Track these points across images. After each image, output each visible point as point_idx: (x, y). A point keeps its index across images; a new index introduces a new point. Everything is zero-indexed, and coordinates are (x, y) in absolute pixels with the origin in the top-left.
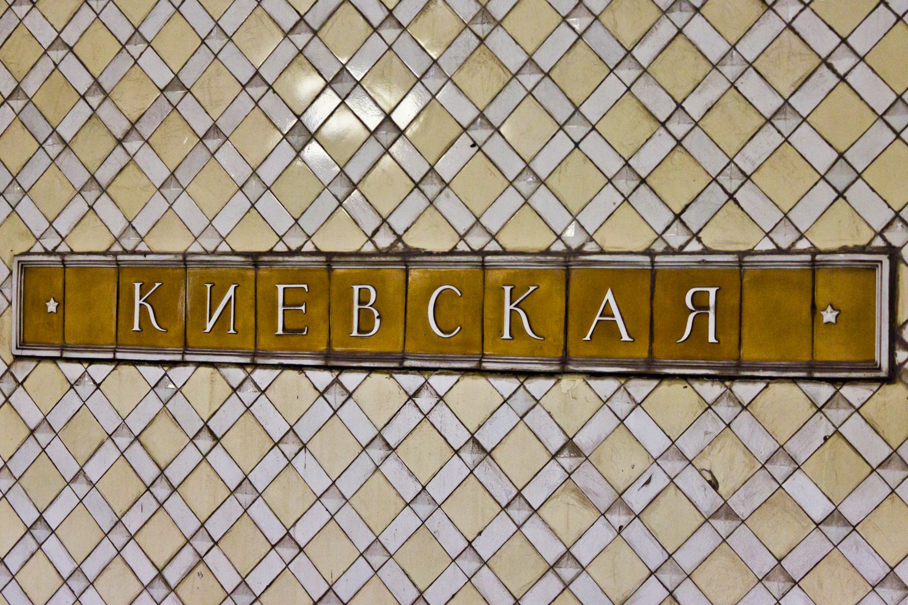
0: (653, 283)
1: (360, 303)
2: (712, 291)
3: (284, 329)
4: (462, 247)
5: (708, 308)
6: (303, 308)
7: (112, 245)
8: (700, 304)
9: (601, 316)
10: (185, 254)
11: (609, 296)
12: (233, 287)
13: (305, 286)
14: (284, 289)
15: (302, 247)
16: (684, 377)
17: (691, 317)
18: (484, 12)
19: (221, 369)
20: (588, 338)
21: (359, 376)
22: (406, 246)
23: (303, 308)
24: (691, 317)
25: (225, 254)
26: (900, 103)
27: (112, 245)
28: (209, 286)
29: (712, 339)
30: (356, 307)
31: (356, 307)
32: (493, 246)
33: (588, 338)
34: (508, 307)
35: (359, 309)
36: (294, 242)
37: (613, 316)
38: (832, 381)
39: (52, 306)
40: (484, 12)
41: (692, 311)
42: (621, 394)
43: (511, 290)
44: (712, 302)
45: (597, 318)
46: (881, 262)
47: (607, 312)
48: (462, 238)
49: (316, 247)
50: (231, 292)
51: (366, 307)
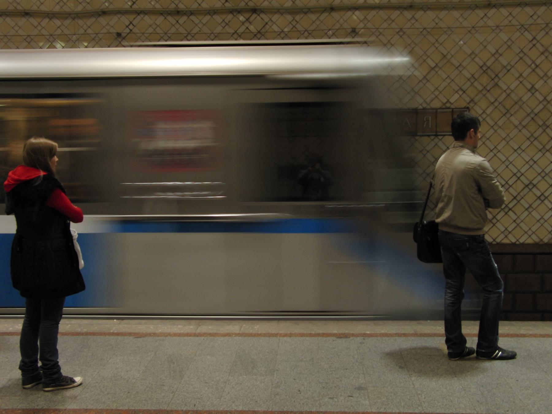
2: (430, 117)
29: (430, 127)
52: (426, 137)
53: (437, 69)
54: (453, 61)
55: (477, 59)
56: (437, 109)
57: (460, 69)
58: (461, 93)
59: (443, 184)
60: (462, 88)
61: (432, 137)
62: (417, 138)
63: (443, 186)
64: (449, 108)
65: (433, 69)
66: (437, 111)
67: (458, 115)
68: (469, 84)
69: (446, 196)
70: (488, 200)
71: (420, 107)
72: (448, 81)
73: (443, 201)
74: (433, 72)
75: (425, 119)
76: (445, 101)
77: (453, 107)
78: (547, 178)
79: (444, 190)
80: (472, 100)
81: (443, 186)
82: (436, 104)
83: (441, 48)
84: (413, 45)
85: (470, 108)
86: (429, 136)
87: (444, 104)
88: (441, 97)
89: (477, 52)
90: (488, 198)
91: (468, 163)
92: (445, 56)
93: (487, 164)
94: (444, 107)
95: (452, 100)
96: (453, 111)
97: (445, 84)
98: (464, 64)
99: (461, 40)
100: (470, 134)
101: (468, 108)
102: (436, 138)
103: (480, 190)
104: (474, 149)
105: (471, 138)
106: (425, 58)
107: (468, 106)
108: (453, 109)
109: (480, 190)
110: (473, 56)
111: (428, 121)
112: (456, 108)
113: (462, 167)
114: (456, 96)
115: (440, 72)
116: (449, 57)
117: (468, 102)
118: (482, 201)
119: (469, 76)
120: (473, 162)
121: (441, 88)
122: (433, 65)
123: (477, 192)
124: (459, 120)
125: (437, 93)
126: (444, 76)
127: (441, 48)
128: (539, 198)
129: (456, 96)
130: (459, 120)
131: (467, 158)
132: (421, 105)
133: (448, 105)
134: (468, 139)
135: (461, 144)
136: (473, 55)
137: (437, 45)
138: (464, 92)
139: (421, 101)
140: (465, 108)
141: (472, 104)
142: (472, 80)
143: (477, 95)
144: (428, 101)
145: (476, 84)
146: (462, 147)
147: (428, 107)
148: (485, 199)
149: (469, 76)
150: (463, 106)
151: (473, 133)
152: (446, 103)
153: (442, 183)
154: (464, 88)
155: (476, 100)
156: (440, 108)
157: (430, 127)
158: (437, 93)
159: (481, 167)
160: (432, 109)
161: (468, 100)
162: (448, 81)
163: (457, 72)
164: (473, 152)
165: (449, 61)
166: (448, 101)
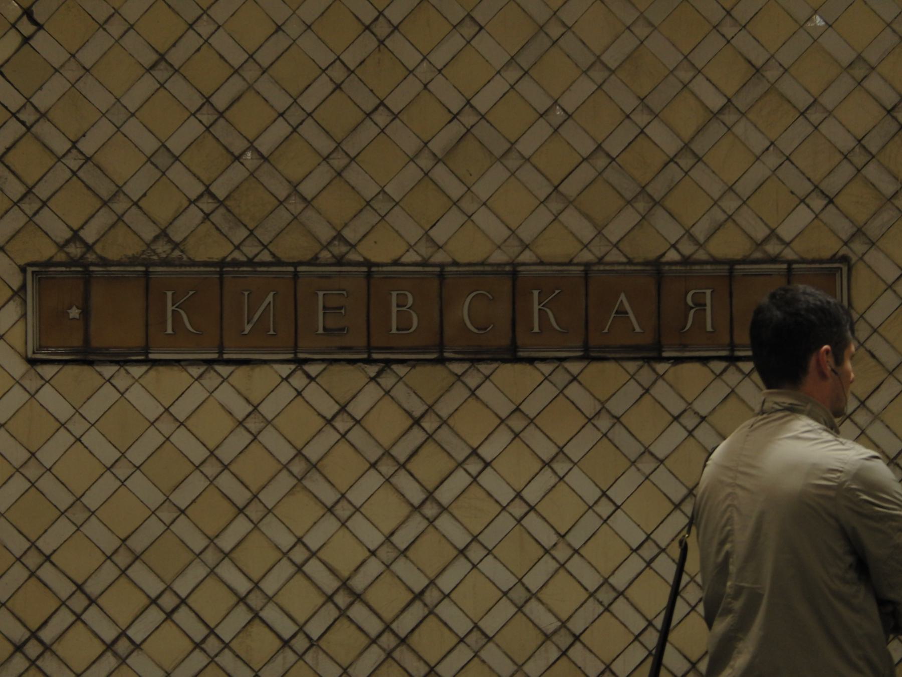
0: (584, 285)
1: (398, 306)
2: (708, 292)
3: (325, 329)
4: (237, 255)
5: (705, 305)
6: (343, 311)
10: (514, 264)
11: (623, 297)
12: (272, 294)
15: (663, 255)
16: (178, 362)
18: (28, 13)
19: (127, 368)
28: (246, 293)
29: (709, 328)
30: (394, 309)
31: (394, 309)
32: (266, 257)
33: (606, 331)
34: (170, 308)
36: (250, 250)
40: (28, 13)
41: (692, 308)
42: (299, 373)
43: (173, 294)
44: (708, 302)
45: (613, 315)
46: (841, 269)
48: (237, 248)
49: (537, 256)
50: (270, 298)
51: (404, 309)
52: (696, 367)
53: (729, 118)
54: (788, 87)
55: (874, 84)
56: (732, 263)
57: (815, 116)
58: (818, 203)
59: (727, 547)
60: (823, 186)
61: (718, 366)
62: (661, 367)
63: (728, 555)
64: (774, 260)
65: (715, 115)
66: (731, 271)
67: (773, 296)
68: (847, 170)
69: (738, 592)
70: (892, 603)
71: (673, 256)
72: (772, 160)
73: (728, 611)
74: (716, 130)
75: (690, 302)
76: (760, 233)
77: (789, 254)
78: (18, 633)
79: (733, 569)
80: (859, 232)
81: (728, 555)
82: (729, 246)
83: (743, 41)
84: (641, 30)
85: (854, 259)
86: (704, 360)
87: (759, 245)
88: (746, 219)
89: (872, 57)
90: (892, 596)
91: (815, 469)
92: (758, 71)
93: (882, 471)
94: (758, 255)
95: (787, 231)
96: (789, 270)
97: (760, 172)
98: (828, 100)
99: (816, 12)
100: (818, 361)
101: (845, 259)
102: (732, 369)
103: (862, 567)
104: (833, 418)
105: (823, 376)
106: (685, 75)
107: (845, 251)
108: (790, 263)
109: (862, 567)
110: (859, 72)
111: (701, 305)
112: (803, 261)
113: (794, 483)
114: (803, 216)
115: (739, 129)
116: (772, 74)
117: (845, 237)
118: (872, 608)
119: (846, 142)
120: (836, 465)
121: (744, 188)
122: (715, 102)
123: (852, 575)
124: (778, 314)
125: (730, 204)
126: (758, 143)
127: (743, 41)
128: (110, 647)
129: (803, 216)
130: (778, 314)
131: (808, 449)
132: (674, 246)
133: (773, 248)
134: (811, 381)
135: (787, 401)
136: (860, 68)
137: (729, 30)
138: (831, 201)
139: (673, 232)
140: (832, 259)
141: (858, 247)
142: (859, 158)
143: (875, 215)
144: (700, 232)
145: (872, 172)
146: (792, 410)
147: (701, 255)
148: (882, 603)
149: (846, 142)
150: (827, 254)
151: (831, 360)
152: (766, 240)
153: (722, 543)
154: (831, 185)
155: (873, 230)
156: (744, 261)
157: (709, 328)
158: (730, 204)
159: (864, 480)
160: (715, 261)
161: (845, 229)
162: (772, 160)
163: (802, 128)
164: (833, 429)
165: (772, 88)
166: (773, 234)
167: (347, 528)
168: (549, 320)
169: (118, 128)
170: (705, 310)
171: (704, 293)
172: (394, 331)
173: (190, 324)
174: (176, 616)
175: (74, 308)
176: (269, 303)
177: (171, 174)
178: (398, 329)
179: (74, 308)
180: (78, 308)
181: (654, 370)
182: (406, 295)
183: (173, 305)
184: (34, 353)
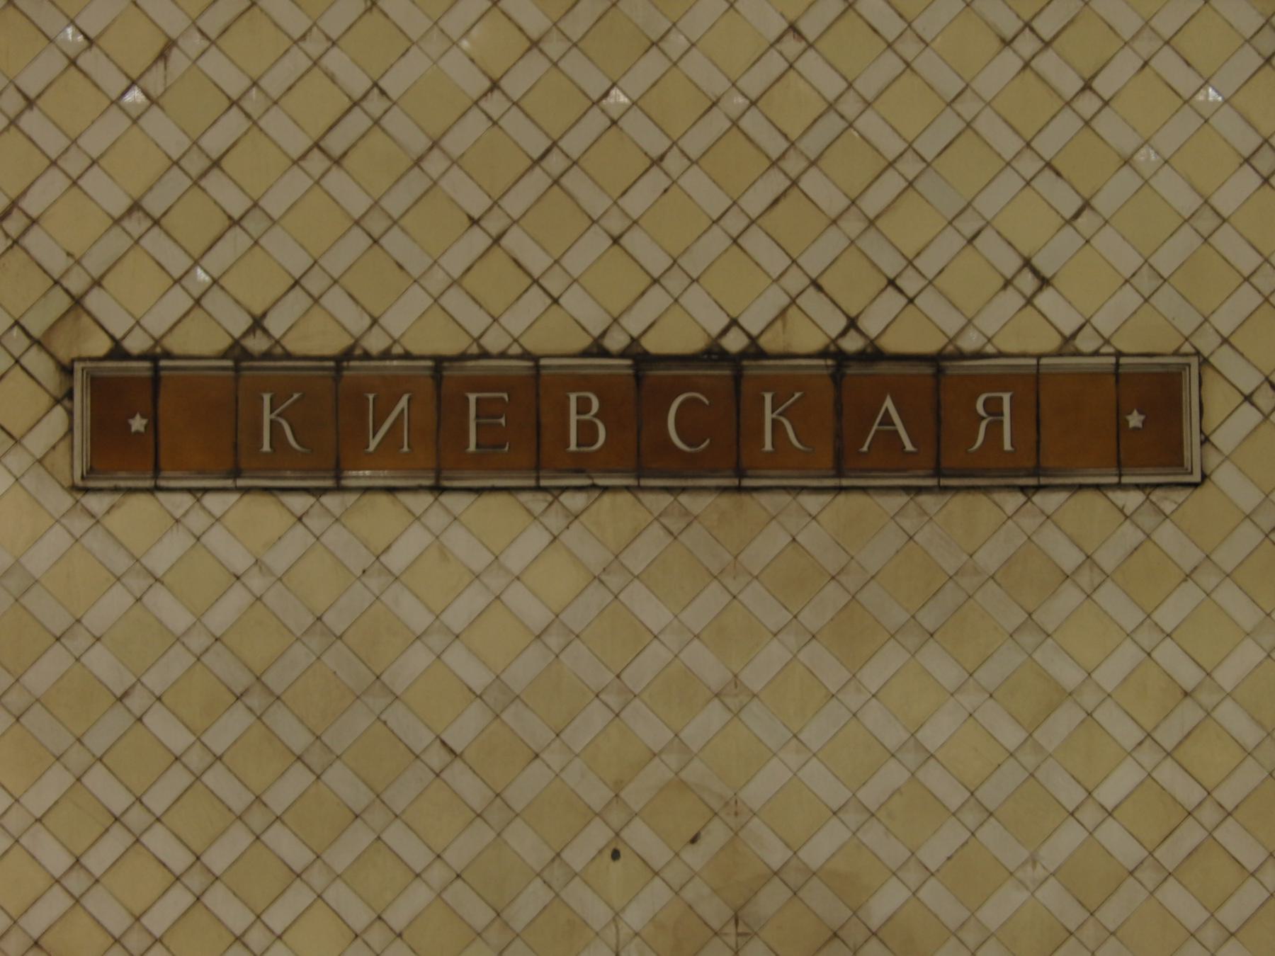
1: (578, 413)
2: (1006, 397)
3: (478, 446)
5: (1002, 414)
7: (510, 346)
8: (994, 408)
9: (880, 424)
11: (889, 404)
12: (405, 398)
13: (505, 396)
14: (478, 400)
17: (983, 425)
20: (406, 449)
21: (1061, 496)
22: (283, 348)
23: (503, 421)
24: (983, 425)
25: (400, 357)
26: (1266, 147)
27: (510, 346)
29: (1007, 446)
31: (573, 418)
33: (406, 449)
35: (578, 421)
37: (893, 424)
38: (1023, 489)
39: (1135, 420)
41: (983, 418)
45: (875, 427)
46: (1189, 365)
47: (887, 420)
50: (403, 403)
51: (587, 417)
167: (80, 188)
168: (786, 434)
169: (1028, 145)
170: (1001, 422)
171: (1001, 399)
172: (573, 447)
173: (296, 439)
174: (65, 142)
175: (138, 417)
176: (403, 410)
177: (1247, 527)
178: (578, 445)
179: (138, 417)
180: (143, 416)
181: (521, 346)
182: (689, 445)
183: (272, 412)
184: (83, 478)
